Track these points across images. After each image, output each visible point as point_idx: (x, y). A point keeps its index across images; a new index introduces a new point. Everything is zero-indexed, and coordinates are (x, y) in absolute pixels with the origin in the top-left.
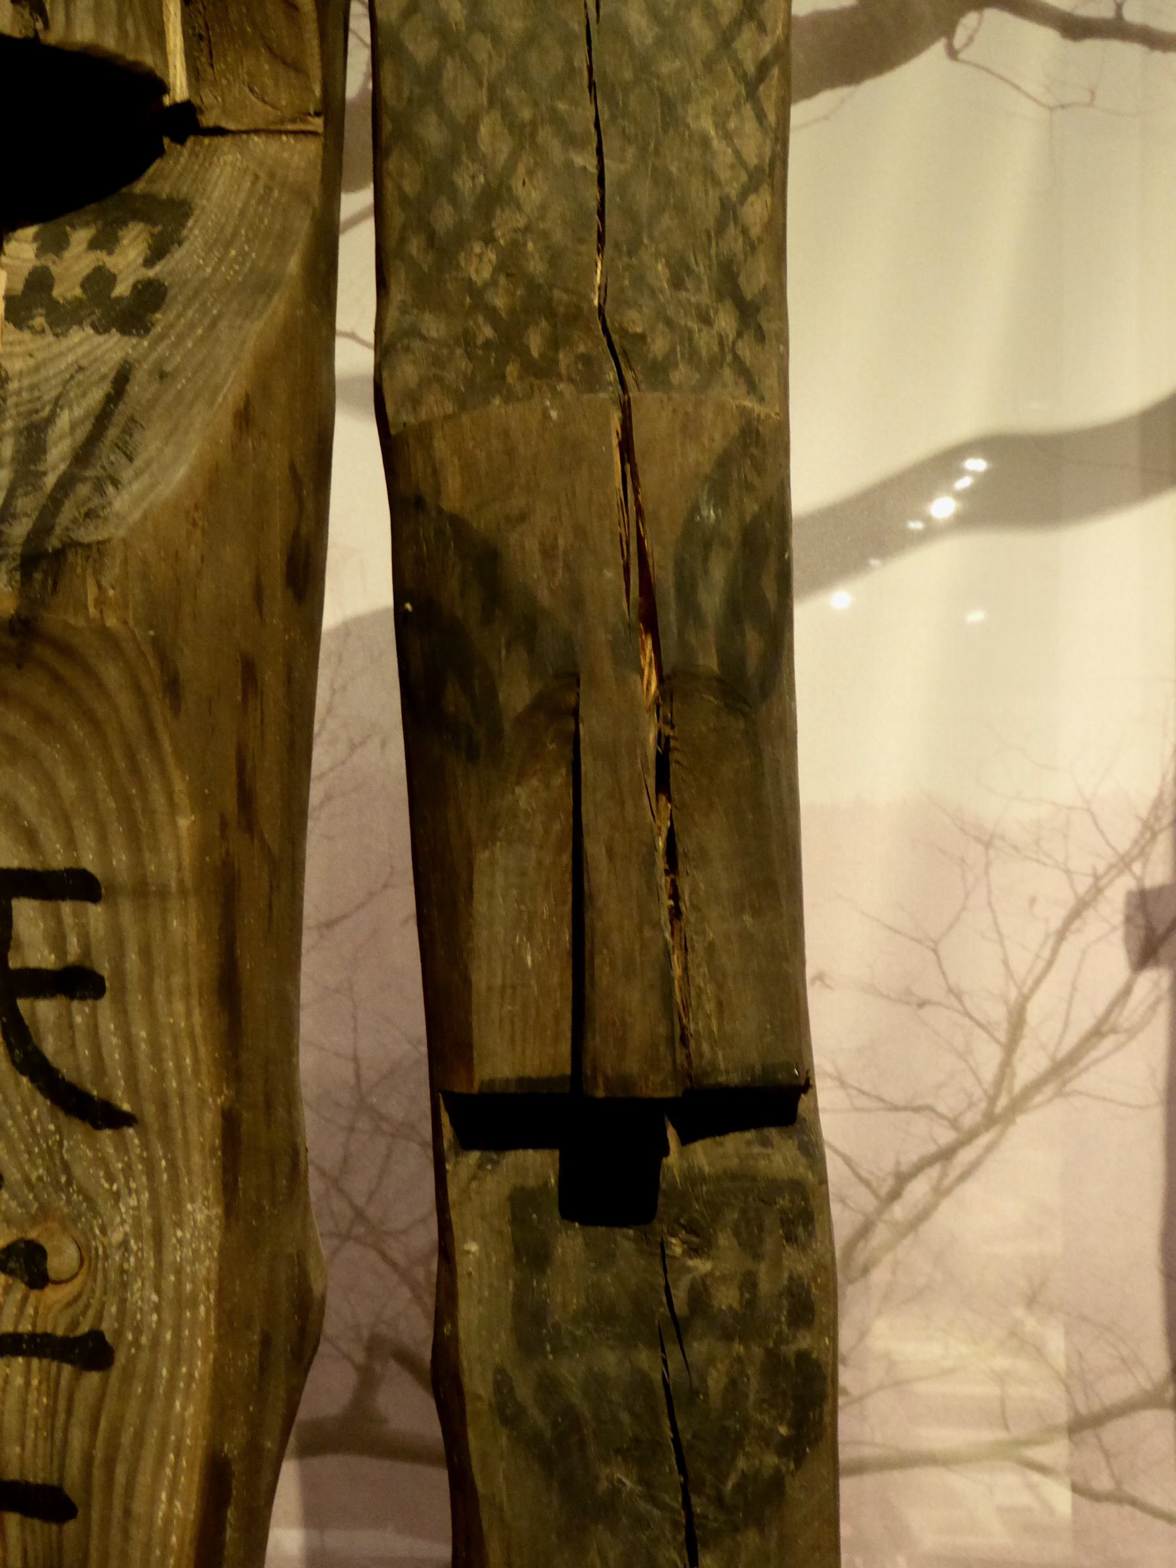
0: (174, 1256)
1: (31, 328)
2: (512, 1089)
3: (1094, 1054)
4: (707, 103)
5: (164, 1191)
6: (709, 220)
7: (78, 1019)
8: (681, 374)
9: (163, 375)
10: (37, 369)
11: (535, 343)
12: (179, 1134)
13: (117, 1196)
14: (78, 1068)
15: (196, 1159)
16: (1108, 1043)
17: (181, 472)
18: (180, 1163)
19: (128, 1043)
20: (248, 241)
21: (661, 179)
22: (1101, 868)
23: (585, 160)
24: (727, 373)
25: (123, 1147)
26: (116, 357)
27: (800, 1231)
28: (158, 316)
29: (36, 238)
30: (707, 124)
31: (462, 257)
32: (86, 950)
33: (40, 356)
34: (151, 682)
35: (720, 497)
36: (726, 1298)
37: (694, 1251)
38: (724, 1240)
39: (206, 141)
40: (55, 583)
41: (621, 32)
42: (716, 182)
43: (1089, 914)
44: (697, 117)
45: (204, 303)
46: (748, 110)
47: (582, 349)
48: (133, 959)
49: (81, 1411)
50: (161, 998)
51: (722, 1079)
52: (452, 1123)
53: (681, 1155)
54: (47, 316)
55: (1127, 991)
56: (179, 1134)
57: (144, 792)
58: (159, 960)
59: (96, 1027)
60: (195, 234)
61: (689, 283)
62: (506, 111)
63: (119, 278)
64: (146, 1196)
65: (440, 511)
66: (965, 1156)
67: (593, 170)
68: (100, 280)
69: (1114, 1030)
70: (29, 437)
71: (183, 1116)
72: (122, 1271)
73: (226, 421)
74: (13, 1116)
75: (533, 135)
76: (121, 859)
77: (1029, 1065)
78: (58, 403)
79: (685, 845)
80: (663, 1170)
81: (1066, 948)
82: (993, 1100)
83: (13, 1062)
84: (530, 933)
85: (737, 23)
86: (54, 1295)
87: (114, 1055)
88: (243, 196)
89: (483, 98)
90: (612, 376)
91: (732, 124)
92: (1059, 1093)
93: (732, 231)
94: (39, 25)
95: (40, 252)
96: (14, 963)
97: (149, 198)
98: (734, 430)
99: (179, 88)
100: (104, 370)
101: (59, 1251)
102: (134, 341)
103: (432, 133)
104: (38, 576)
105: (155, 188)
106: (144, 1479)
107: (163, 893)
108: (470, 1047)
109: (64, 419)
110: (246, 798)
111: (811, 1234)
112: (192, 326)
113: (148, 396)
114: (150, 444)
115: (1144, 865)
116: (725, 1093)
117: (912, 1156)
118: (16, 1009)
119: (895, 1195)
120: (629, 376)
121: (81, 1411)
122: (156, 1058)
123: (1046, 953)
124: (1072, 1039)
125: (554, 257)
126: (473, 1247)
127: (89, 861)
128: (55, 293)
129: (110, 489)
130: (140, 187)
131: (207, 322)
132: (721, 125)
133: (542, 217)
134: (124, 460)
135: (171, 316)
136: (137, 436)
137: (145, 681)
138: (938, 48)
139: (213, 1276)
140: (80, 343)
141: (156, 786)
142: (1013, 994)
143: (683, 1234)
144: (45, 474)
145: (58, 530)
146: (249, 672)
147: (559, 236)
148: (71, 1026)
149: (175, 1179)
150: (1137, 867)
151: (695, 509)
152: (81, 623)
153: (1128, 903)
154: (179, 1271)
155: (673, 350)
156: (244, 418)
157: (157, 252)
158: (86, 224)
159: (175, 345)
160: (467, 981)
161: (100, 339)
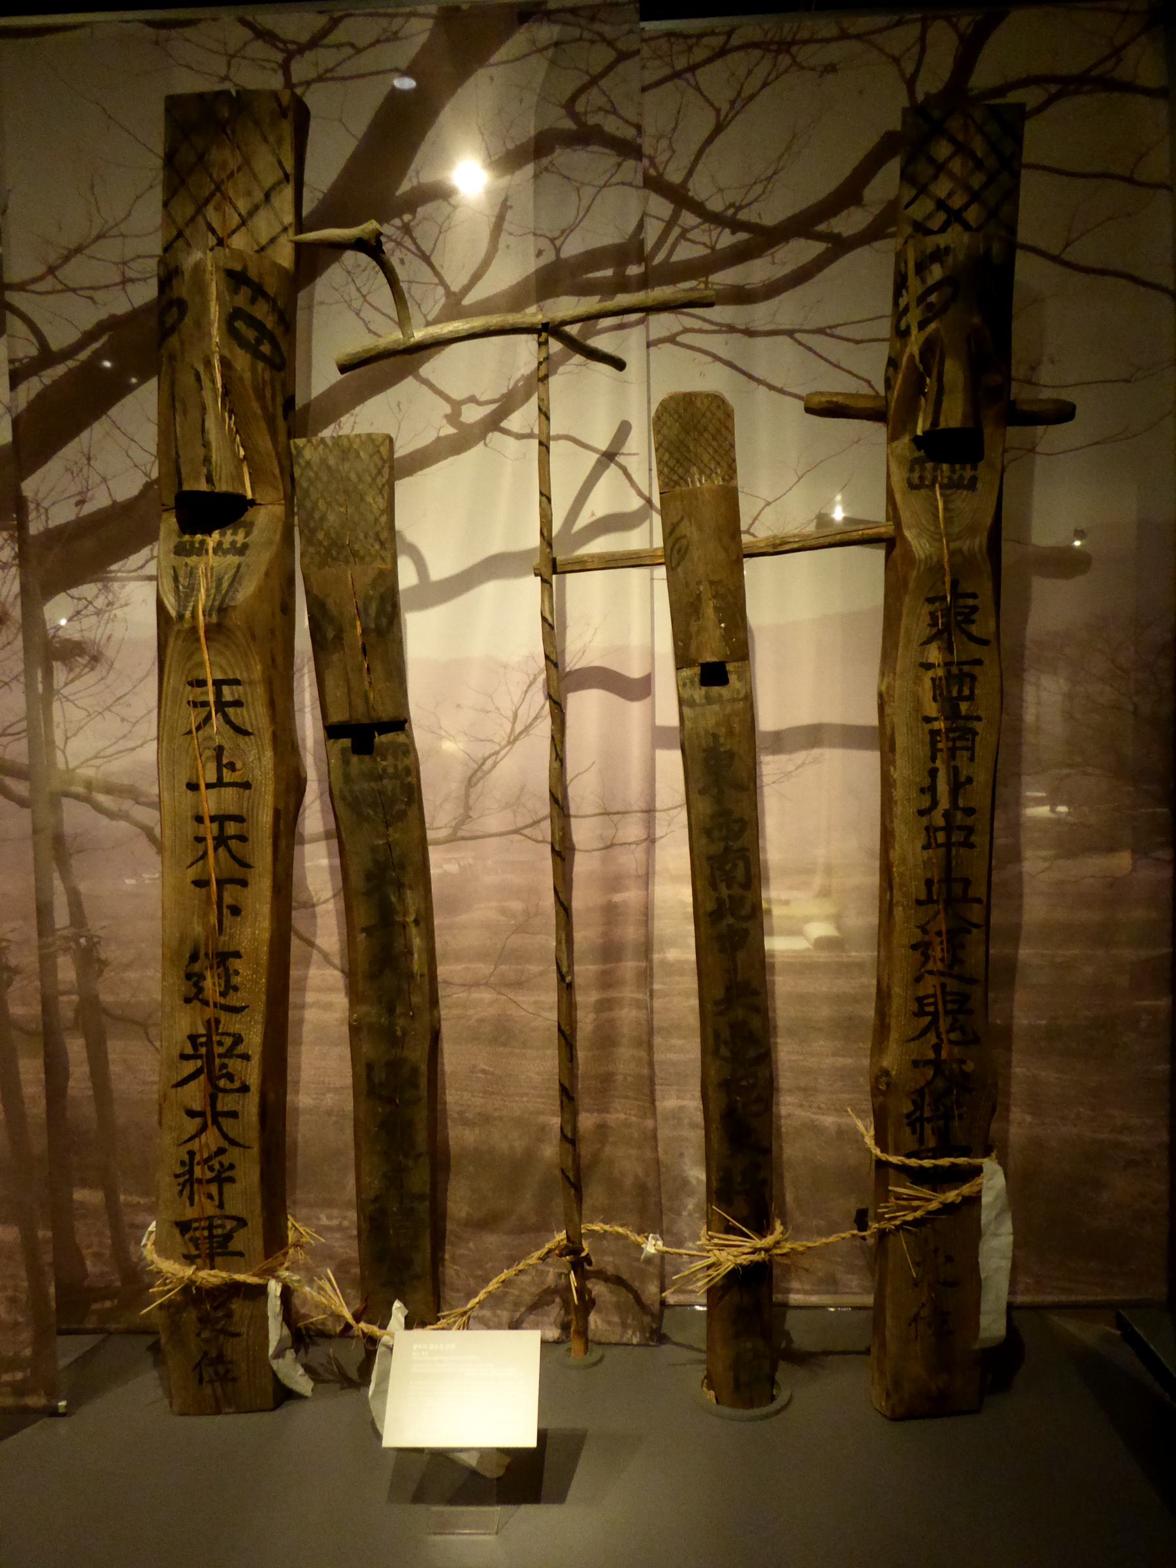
8: (368, 559)
16: (539, 721)
17: (252, 588)
19: (250, 717)
25: (250, 739)
26: (237, 562)
35: (374, 588)
36: (391, 770)
37: (382, 760)
38: (390, 757)
49: (246, 799)
60: (255, 531)
62: (325, 499)
66: (503, 753)
68: (233, 543)
77: (518, 729)
78: (225, 573)
79: (371, 667)
81: (527, 695)
82: (509, 737)
85: (376, 476)
86: (237, 773)
97: (244, 522)
98: (376, 572)
99: (249, 495)
106: (260, 813)
109: (226, 577)
110: (273, 660)
116: (384, 723)
117: (487, 754)
119: (483, 764)
121: (246, 799)
122: (256, 719)
130: (242, 519)
138: (482, 443)
146: (273, 632)
156: (267, 574)
157: (247, 535)
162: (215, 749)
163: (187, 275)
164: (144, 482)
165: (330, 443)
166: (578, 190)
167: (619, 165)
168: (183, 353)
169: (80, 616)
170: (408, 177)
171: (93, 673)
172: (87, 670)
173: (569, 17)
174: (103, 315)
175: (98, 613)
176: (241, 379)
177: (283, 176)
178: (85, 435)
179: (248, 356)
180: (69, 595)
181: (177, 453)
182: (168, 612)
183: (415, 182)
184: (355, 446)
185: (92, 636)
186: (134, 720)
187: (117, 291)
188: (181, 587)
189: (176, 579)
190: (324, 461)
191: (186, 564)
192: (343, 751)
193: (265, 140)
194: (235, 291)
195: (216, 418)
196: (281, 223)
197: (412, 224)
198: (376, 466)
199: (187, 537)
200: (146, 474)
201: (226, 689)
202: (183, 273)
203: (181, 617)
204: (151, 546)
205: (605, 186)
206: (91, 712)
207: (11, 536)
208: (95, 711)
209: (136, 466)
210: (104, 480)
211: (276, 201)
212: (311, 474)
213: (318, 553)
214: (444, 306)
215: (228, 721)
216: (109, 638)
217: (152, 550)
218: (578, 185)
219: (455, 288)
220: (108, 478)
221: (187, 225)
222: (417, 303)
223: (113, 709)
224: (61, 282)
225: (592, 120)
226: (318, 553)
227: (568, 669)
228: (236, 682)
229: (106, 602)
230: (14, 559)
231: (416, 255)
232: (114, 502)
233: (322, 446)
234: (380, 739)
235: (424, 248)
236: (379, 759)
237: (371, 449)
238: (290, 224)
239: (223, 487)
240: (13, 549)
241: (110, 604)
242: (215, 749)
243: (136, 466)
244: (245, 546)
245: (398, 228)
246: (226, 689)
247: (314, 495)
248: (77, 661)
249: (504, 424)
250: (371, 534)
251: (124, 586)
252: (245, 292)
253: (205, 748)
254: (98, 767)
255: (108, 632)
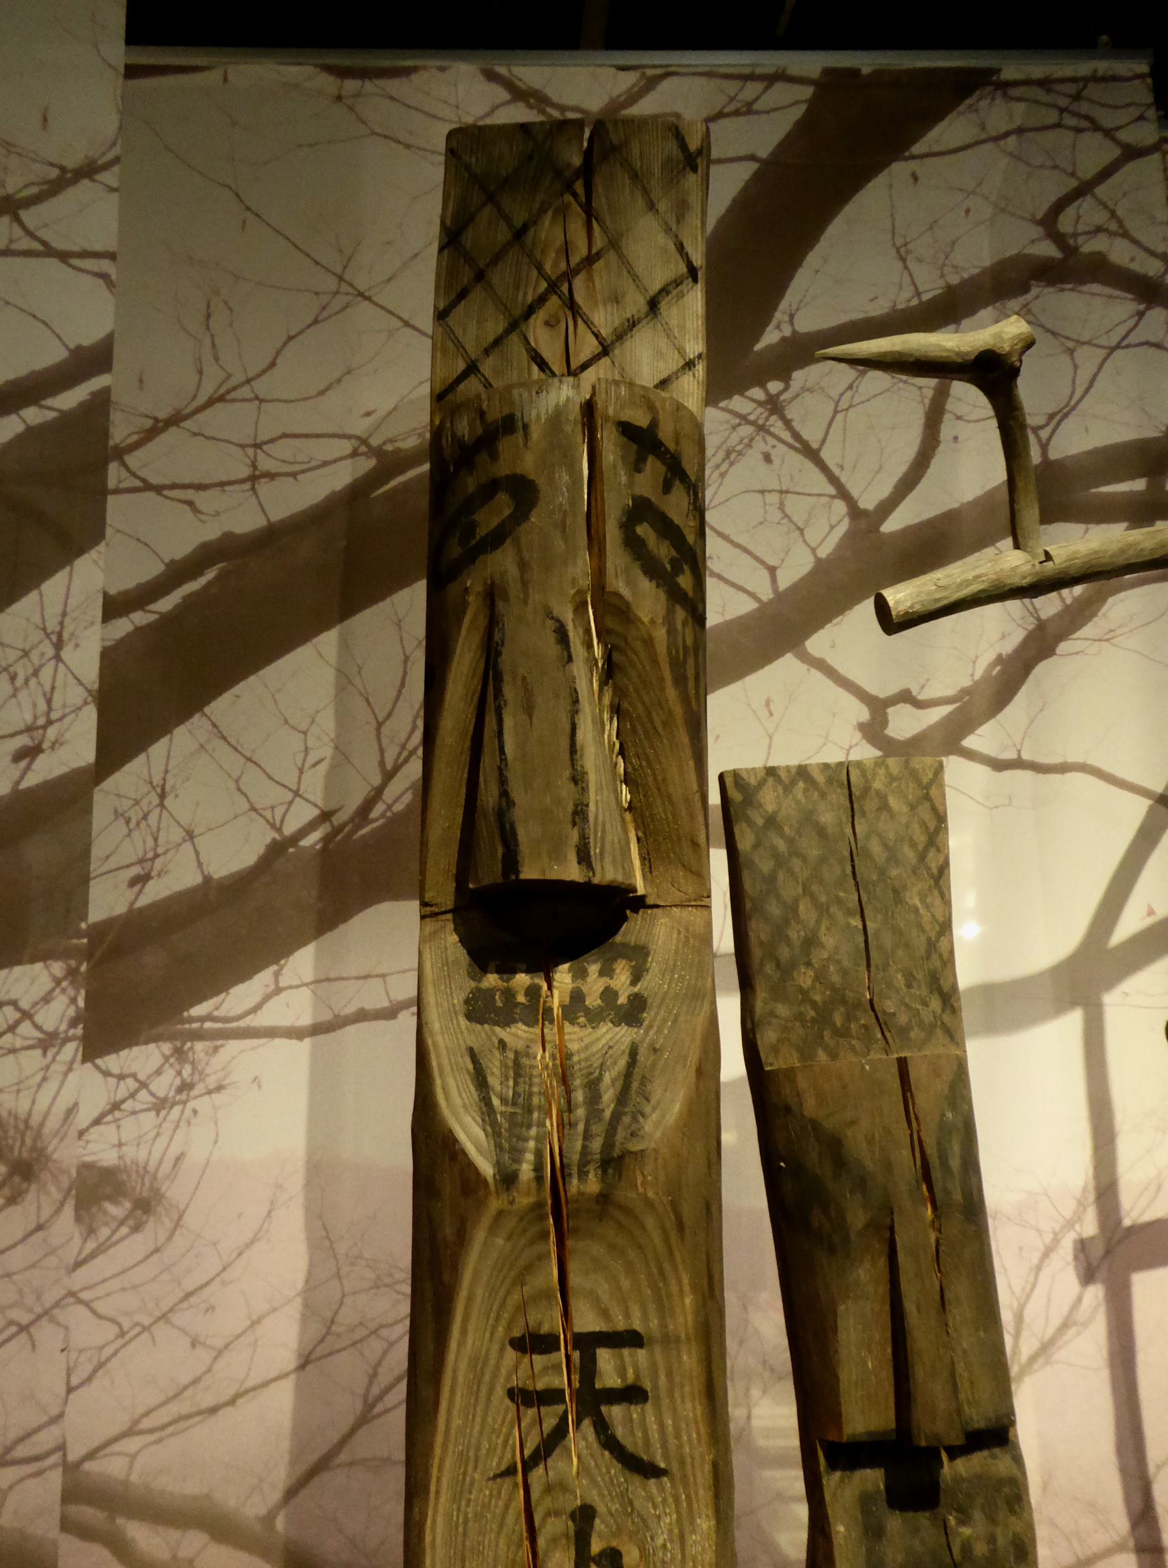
0: (692, 1550)
1: (578, 1024)
2: (865, 1439)
3: (1065, 1338)
4: (915, 890)
5: (684, 1512)
6: (922, 951)
7: (635, 1416)
9: (655, 1050)
10: (587, 1047)
11: (838, 1019)
12: (691, 1478)
13: (659, 1517)
14: (636, 1444)
15: (701, 1492)
16: (1072, 1331)
17: (677, 1108)
18: (693, 1496)
20: (683, 969)
21: (897, 932)
22: (1057, 1228)
23: (856, 922)
24: (939, 1032)
25: (662, 1489)
26: (627, 1040)
27: (1016, 1507)
28: (645, 1015)
29: (570, 970)
30: (916, 901)
31: (795, 974)
32: (637, 1376)
33: (587, 1040)
34: (670, 1224)
37: (961, 1522)
38: (977, 1515)
39: (649, 911)
40: (620, 1176)
41: (868, 855)
42: (924, 931)
43: (1054, 1256)
44: (911, 898)
45: (668, 1007)
46: (936, 892)
47: (863, 1022)
48: (663, 1380)
50: (679, 1401)
51: (976, 1426)
52: (826, 1457)
53: (950, 1468)
54: (585, 1016)
55: (1079, 1300)
56: (691, 1478)
57: (667, 1285)
58: (677, 1379)
59: (645, 1419)
60: (654, 966)
61: (915, 985)
62: (813, 897)
63: (620, 992)
64: (674, 1517)
65: (803, 1115)
67: (861, 927)
68: (609, 994)
69: (1075, 1324)
70: (590, 1088)
71: (693, 1467)
72: (663, 1562)
73: (692, 1074)
74: (601, 1474)
75: (828, 908)
76: (654, 1323)
80: (942, 1477)
83: (600, 1443)
84: (870, 1351)
87: (655, 1436)
88: (674, 942)
89: (800, 890)
90: (879, 1036)
91: (928, 900)
92: (1047, 1363)
93: (935, 957)
94: (591, 874)
95: (574, 978)
96: (598, 1386)
97: (625, 945)
100: (623, 1048)
101: (629, 1552)
102: (636, 1030)
103: (774, 909)
104: (610, 1171)
105: (627, 940)
107: (678, 1340)
108: (840, 1415)
109: (607, 1078)
111: (1022, 1509)
112: (665, 1021)
113: (649, 1063)
114: (657, 1090)
115: (1081, 1226)
118: (600, 1412)
120: (888, 1035)
122: (678, 1436)
123: (1032, 1279)
124: (1050, 1331)
125: (844, 973)
126: (841, 1529)
127: (637, 1326)
128: (587, 1003)
129: (641, 1119)
130: (618, 938)
131: (672, 1018)
132: (923, 901)
133: (837, 953)
134: (645, 1101)
135: (652, 1013)
136: (649, 1087)
137: (668, 1225)
139: (714, 1561)
140: (607, 1032)
141: (673, 1282)
142: (1015, 1305)
143: (954, 1513)
144: (603, 1110)
145: (617, 1144)
147: (846, 963)
148: (631, 1420)
149: (690, 1504)
150: (1077, 1227)
151: (943, 1115)
152: (634, 1196)
153: (1075, 1249)
154: (694, 1561)
155: (910, 1021)
157: (636, 979)
158: (595, 962)
159: (659, 1031)
160: (837, 1378)
161: (617, 1029)
162: (573, 1516)
163: (535, 434)
164: (268, 840)
165: (820, 779)
166: (1071, 352)
167: (1141, 315)
168: (525, 584)
169: (117, 1114)
170: (774, 322)
171: (139, 1237)
172: (124, 1230)
173: (1039, 94)
174: (211, 532)
175: (161, 1105)
176: (649, 642)
177: (685, 270)
178: (158, 749)
179: (663, 596)
180: (97, 1067)
181: (504, 794)
182: (471, 1165)
183: (787, 331)
184: (877, 785)
185: (142, 1155)
186: (219, 1343)
187: (238, 493)
188: (496, 1102)
189: (480, 1080)
190: (808, 818)
191: (502, 1044)
192: (865, 1500)
193: (651, 206)
194: (637, 467)
195: (594, 722)
196: (681, 351)
197: (782, 398)
198: (923, 824)
199: (492, 980)
200: (273, 826)
201: (605, 1358)
202: (526, 427)
203: (508, 1179)
204: (274, 968)
205: (1118, 346)
206: (126, 1325)
207: (72, 973)
208: (137, 1324)
209: (253, 809)
210: (190, 835)
211: (670, 312)
212: (781, 845)
213: (800, 1017)
214: (848, 535)
215: (610, 1443)
216: (178, 1159)
217: (277, 975)
218: (1071, 344)
219: (868, 503)
220: (196, 832)
221: (487, 352)
222: (798, 528)
223: (177, 1319)
224: (134, 475)
225: (1089, 246)
226: (800, 1017)
227: (1127, 1222)
228: (633, 1339)
229: (178, 1081)
230: (73, 1023)
231: (791, 446)
232: (207, 880)
233: (801, 785)
234: (952, 1470)
235: (805, 435)
236: (952, 1521)
237: (912, 792)
238: (700, 356)
239: (607, 873)
240: (73, 1001)
241: (185, 1087)
242: (573, 1516)
243: (253, 809)
244: (638, 1005)
245: (760, 403)
246: (605, 1358)
247: (789, 890)
248: (105, 1213)
249: (970, 742)
250: (920, 976)
251: (216, 1049)
252: (653, 467)
253: (548, 1514)
254: (133, 1457)
255: (174, 1151)
